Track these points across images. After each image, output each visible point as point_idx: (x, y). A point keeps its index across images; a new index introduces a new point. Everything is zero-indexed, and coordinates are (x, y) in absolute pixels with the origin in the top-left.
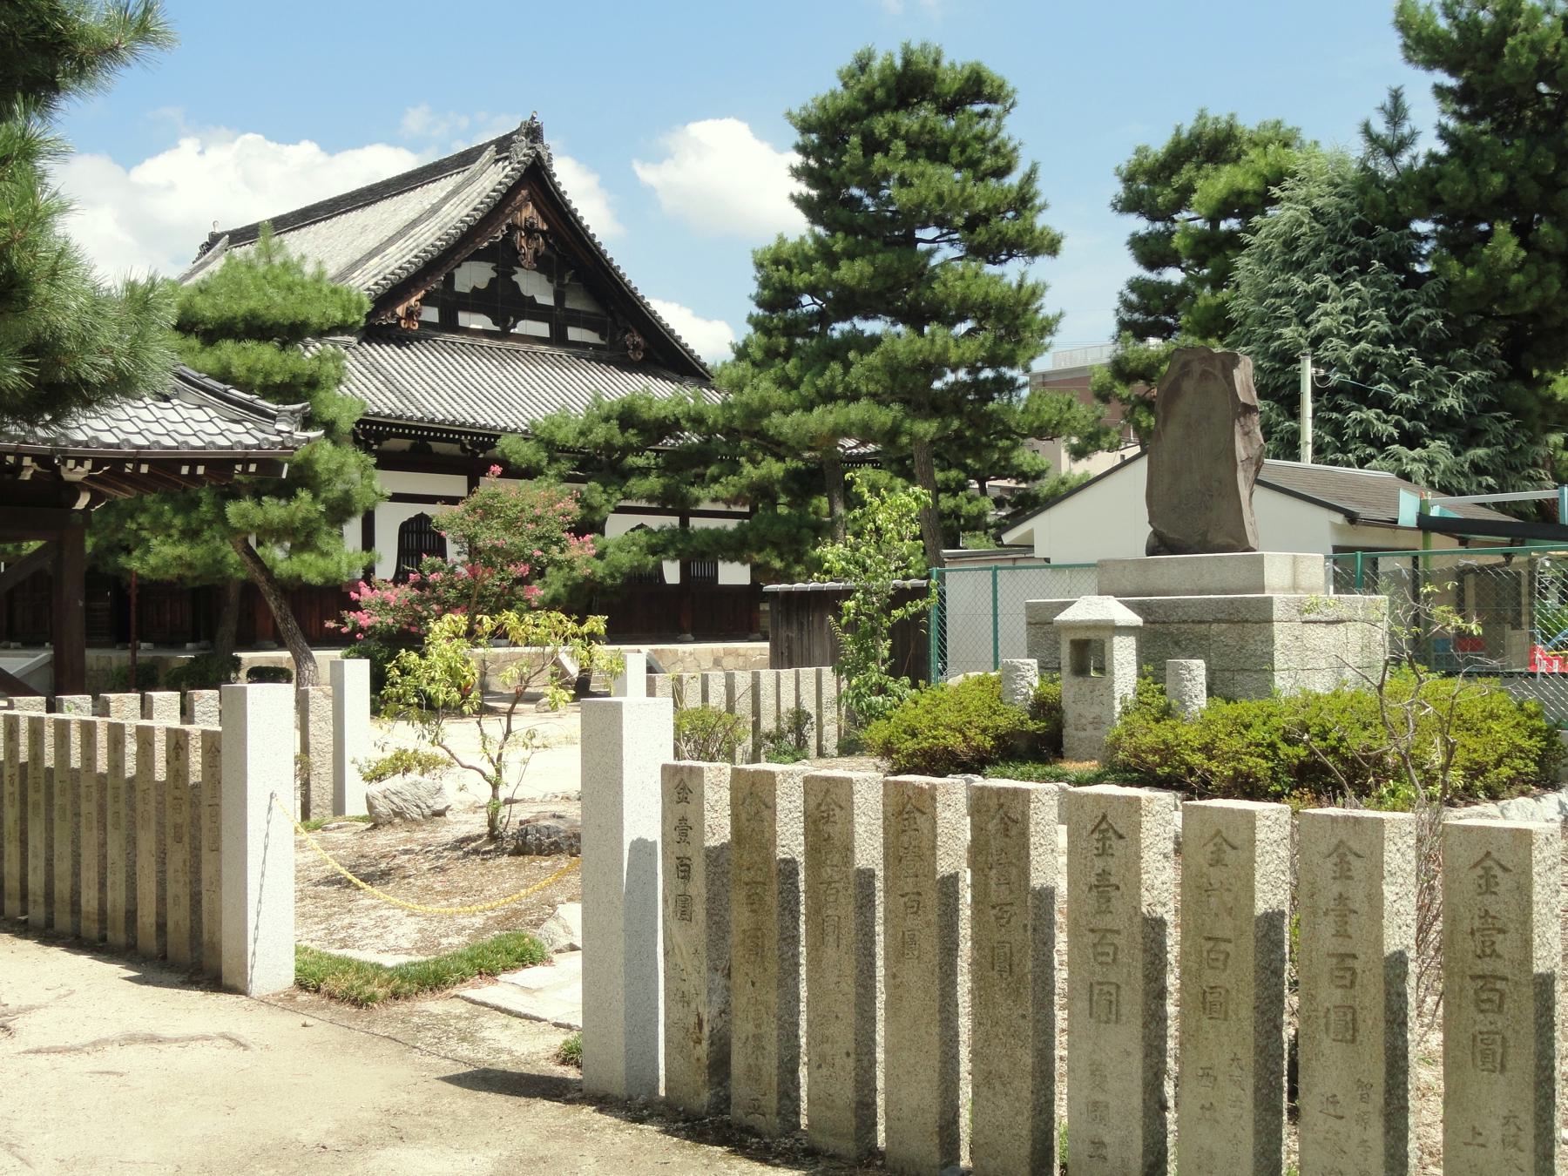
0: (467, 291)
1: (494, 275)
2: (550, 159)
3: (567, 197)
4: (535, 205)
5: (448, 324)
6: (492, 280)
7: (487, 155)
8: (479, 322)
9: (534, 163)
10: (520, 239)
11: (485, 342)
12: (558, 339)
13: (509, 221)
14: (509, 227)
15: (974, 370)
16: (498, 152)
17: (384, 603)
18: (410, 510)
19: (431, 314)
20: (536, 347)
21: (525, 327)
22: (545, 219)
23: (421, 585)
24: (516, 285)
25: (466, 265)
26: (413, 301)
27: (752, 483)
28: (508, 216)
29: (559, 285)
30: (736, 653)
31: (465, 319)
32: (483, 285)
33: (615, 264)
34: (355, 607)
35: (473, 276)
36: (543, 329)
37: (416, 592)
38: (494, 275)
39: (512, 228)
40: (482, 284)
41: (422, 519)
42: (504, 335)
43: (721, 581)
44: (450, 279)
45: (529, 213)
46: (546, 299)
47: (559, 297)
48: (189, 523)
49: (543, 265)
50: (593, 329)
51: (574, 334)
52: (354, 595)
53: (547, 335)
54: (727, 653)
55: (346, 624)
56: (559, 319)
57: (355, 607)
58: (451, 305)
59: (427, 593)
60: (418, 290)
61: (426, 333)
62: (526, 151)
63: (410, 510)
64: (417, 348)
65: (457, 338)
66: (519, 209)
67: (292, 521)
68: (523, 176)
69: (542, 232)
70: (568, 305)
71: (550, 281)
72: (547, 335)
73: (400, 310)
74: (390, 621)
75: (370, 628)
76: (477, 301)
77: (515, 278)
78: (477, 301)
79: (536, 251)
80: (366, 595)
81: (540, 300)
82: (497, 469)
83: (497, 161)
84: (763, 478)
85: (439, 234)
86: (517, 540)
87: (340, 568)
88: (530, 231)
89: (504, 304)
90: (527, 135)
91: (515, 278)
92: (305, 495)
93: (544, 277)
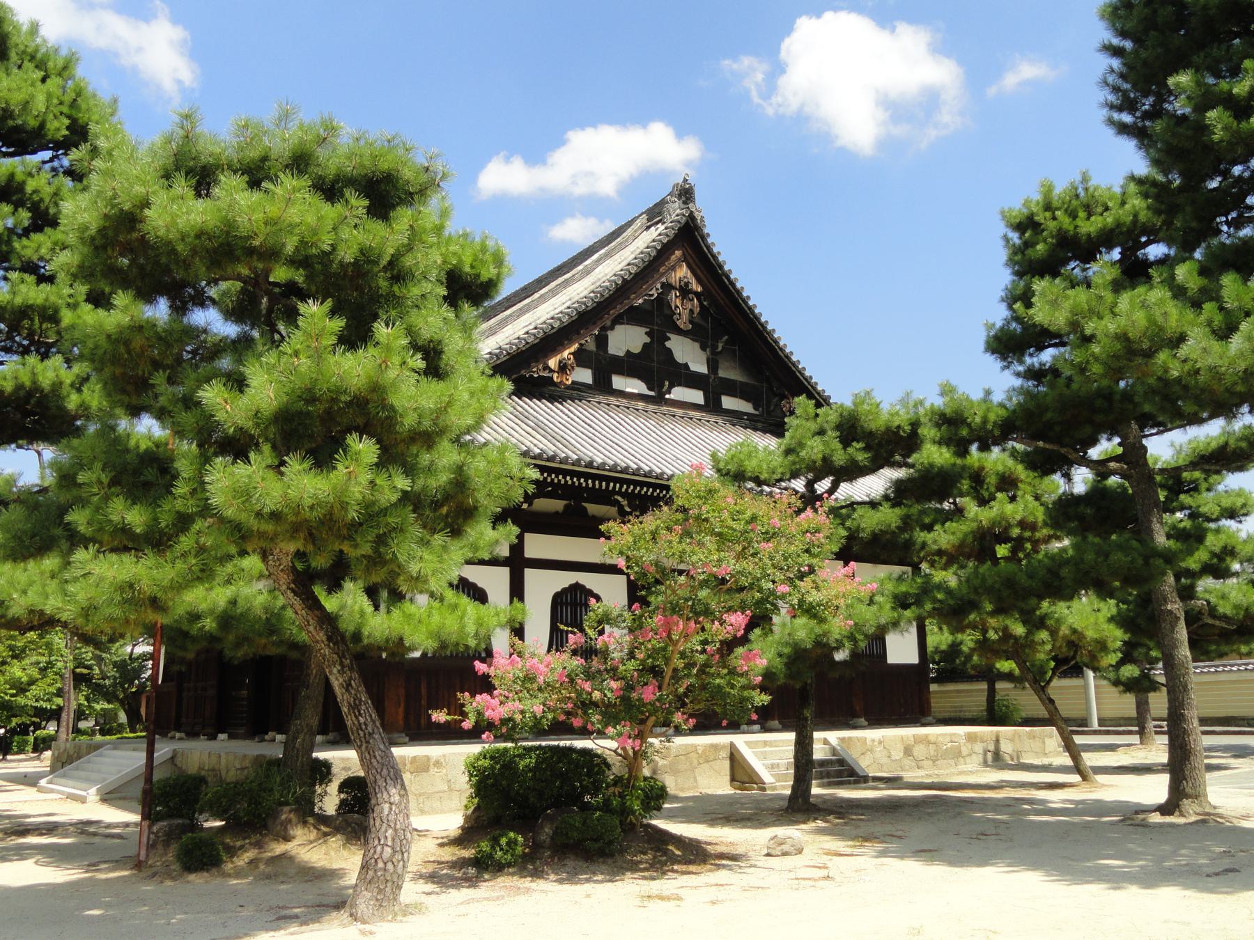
0: (622, 354)
1: (648, 340)
2: (702, 221)
3: (721, 259)
4: (689, 266)
5: (602, 386)
6: (645, 345)
7: (638, 223)
8: (635, 386)
9: (687, 223)
10: (674, 299)
11: (641, 405)
12: (712, 406)
13: (664, 280)
14: (663, 285)
16: (648, 220)
17: (529, 678)
18: (565, 579)
19: (585, 376)
20: (692, 413)
21: (678, 393)
22: (699, 281)
23: (587, 652)
24: (669, 351)
25: (619, 328)
26: (566, 354)
27: (980, 528)
28: (662, 275)
29: (714, 353)
30: (926, 741)
31: (618, 382)
33: (769, 328)
34: (485, 685)
35: (626, 339)
36: (697, 396)
37: (577, 662)
38: (648, 340)
39: (667, 287)
40: (636, 349)
41: (576, 588)
42: (659, 400)
44: (602, 341)
45: (682, 273)
46: (699, 366)
47: (713, 365)
48: (156, 519)
49: (694, 333)
50: (747, 399)
51: (728, 402)
52: (480, 667)
53: (702, 402)
54: (919, 740)
55: (464, 715)
56: (713, 388)
57: (485, 685)
58: (605, 369)
59: (596, 663)
60: (571, 342)
61: (577, 393)
62: (678, 211)
63: (565, 579)
64: (569, 404)
65: (612, 400)
66: (673, 268)
67: (344, 506)
68: (676, 236)
69: (696, 294)
70: (722, 373)
71: (703, 348)
72: (702, 402)
73: (553, 363)
74: (538, 709)
75: (504, 721)
76: (630, 365)
77: (668, 344)
78: (630, 365)
79: (691, 311)
80: (502, 667)
83: (648, 228)
84: (994, 523)
85: (592, 287)
86: (749, 565)
87: (463, 627)
88: (685, 291)
89: (658, 371)
90: (680, 197)
91: (668, 344)
92: (365, 449)
93: (697, 345)
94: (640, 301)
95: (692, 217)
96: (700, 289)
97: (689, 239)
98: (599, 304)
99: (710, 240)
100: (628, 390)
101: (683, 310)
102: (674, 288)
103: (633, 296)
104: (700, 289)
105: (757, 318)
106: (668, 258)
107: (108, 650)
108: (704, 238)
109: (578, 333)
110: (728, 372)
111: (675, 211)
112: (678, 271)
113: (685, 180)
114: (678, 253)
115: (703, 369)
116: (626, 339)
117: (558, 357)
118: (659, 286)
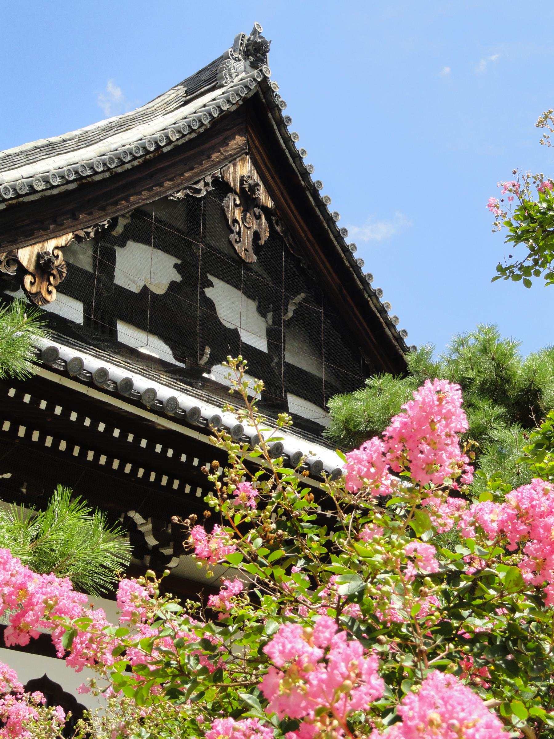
1: (178, 278)
4: (255, 164)
6: (173, 285)
9: (256, 94)
10: (232, 207)
14: (216, 181)
15: (420, 490)
24: (210, 304)
25: (131, 244)
26: (50, 245)
28: (215, 165)
29: (277, 321)
32: (160, 288)
38: (178, 278)
39: (222, 187)
43: (37, 440)
45: (243, 170)
46: (256, 339)
66: (232, 159)
69: (265, 209)
70: (290, 358)
71: (262, 311)
77: (209, 292)
78: (144, 309)
79: (257, 236)
81: (247, 338)
82: (33, 281)
90: (246, 54)
91: (209, 292)
93: (252, 305)
94: (180, 195)
95: (264, 86)
96: (270, 204)
97: (257, 118)
98: (115, 177)
99: (291, 129)
100: (143, 350)
101: (246, 231)
102: (231, 190)
103: (167, 184)
104: (270, 204)
105: (356, 267)
106: (225, 143)
107: (541, 548)
108: (282, 123)
109: (75, 218)
110: (297, 357)
111: (239, 74)
112: (239, 165)
113: (255, 32)
114: (239, 140)
115: (262, 345)
116: (143, 268)
117: (37, 248)
118: (209, 179)
